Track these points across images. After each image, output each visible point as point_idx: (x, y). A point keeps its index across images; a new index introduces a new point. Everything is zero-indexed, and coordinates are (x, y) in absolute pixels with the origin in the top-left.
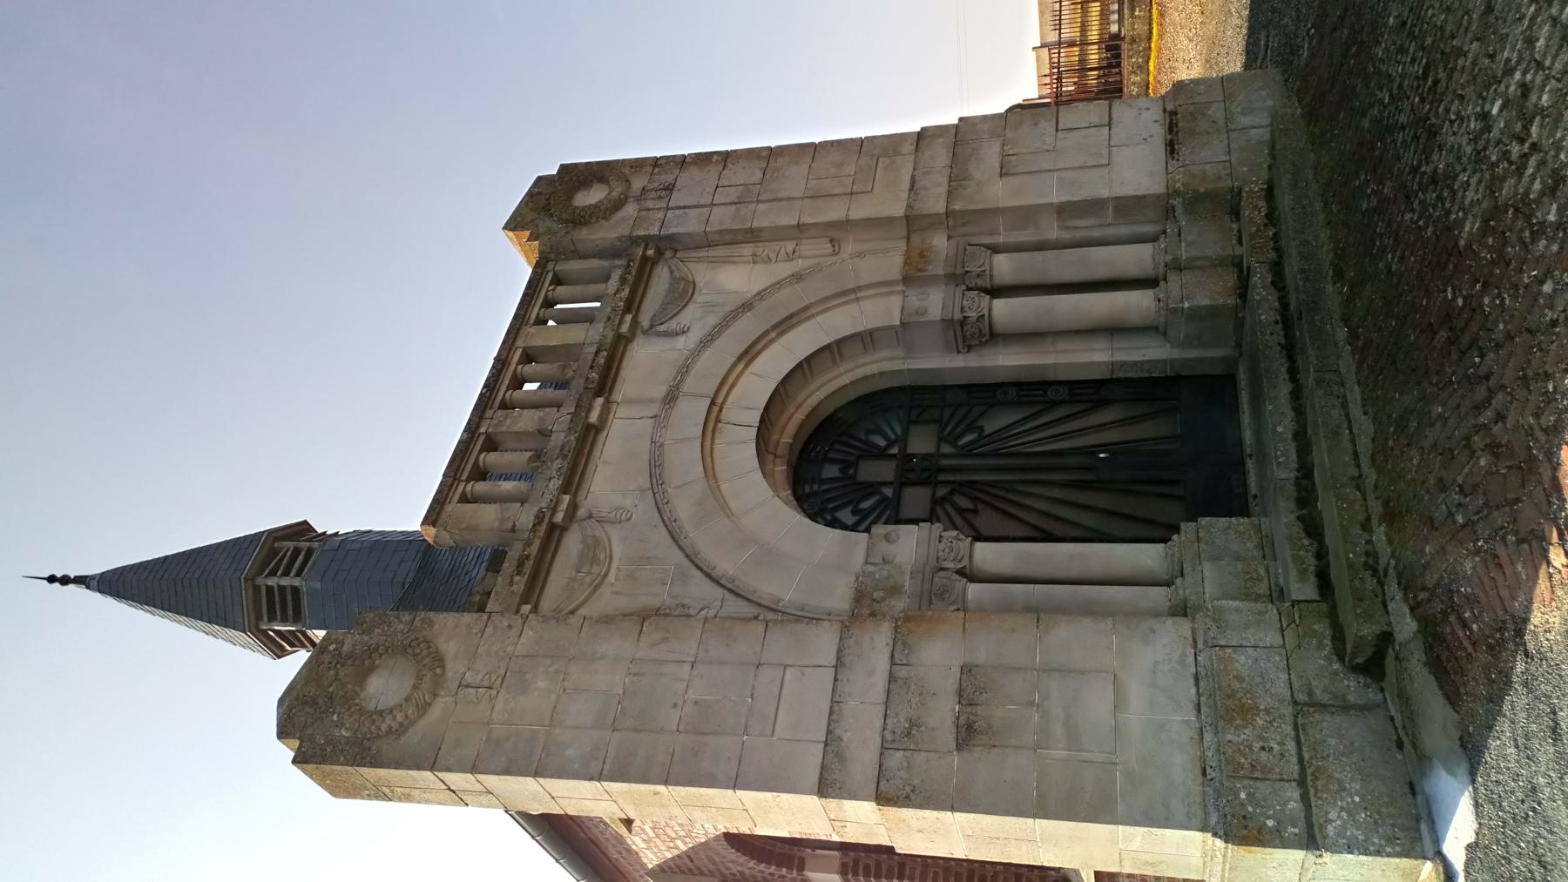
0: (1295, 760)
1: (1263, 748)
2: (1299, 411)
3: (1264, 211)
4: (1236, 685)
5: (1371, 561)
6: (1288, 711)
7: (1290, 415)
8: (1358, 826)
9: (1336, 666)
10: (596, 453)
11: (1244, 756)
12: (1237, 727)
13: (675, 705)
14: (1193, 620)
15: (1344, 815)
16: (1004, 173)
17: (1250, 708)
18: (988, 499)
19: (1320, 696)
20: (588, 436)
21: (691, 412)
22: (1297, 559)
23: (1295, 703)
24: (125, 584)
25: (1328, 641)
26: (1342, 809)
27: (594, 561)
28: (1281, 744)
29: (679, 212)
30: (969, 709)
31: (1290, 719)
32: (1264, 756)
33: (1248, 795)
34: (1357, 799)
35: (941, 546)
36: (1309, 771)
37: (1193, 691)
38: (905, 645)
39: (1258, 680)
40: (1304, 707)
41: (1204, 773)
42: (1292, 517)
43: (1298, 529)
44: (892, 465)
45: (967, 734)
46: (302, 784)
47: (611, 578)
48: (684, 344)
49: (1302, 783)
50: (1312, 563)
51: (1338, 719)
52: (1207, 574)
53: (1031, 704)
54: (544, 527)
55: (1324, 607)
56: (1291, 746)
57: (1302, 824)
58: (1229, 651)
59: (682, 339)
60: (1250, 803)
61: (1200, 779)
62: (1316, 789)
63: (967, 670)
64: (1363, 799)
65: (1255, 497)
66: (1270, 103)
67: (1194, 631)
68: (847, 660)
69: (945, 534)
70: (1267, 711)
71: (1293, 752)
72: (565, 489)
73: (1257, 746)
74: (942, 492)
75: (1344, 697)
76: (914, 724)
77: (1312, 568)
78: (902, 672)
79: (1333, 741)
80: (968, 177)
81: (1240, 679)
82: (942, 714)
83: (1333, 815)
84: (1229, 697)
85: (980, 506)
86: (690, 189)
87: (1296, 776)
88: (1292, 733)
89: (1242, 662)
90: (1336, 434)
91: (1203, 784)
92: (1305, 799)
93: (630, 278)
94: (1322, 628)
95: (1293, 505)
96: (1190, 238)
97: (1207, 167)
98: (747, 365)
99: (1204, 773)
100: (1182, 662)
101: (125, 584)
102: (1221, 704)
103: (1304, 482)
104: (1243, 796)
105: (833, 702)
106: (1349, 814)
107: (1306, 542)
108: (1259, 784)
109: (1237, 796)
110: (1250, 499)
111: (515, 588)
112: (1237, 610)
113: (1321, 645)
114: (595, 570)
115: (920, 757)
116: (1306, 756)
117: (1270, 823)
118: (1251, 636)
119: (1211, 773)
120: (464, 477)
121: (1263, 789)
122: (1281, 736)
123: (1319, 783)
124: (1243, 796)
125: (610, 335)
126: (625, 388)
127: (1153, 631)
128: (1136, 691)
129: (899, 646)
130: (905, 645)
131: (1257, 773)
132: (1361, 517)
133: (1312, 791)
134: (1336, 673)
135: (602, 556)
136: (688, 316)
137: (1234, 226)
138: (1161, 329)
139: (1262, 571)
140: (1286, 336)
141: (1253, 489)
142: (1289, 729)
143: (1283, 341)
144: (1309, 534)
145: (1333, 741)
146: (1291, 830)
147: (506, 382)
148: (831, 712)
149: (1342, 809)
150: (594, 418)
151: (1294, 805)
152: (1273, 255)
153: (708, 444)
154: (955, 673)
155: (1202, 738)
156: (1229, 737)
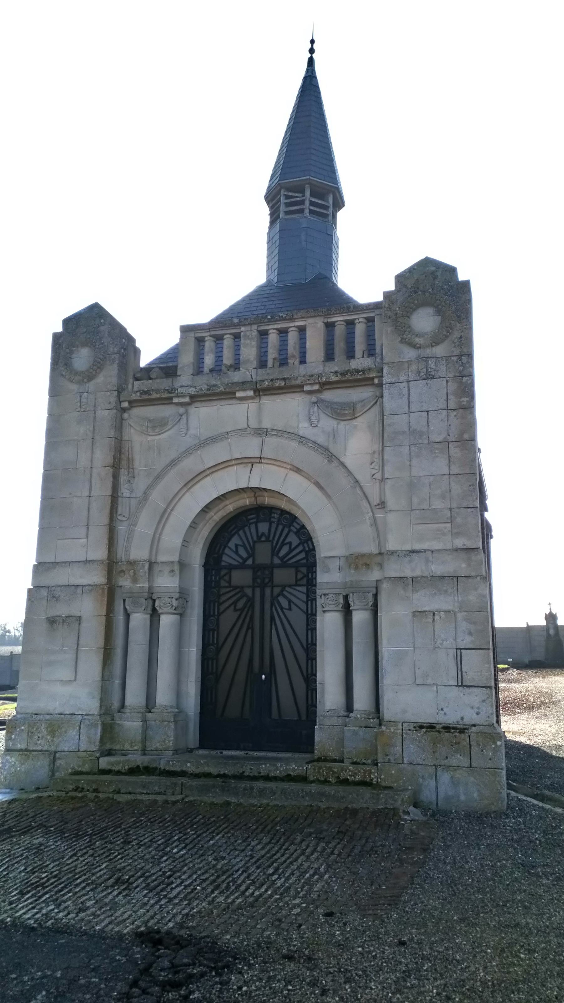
0: (35, 749)
1: (39, 737)
2: (197, 776)
3: (351, 779)
4: (64, 730)
5: (80, 789)
6: (53, 749)
7: (197, 771)
8: (10, 767)
9: (70, 771)
10: (223, 402)
11: (36, 730)
12: (47, 729)
13: (71, 494)
14: (97, 715)
15: (13, 763)
16: (418, 614)
17: (54, 734)
18: (243, 616)
19: (58, 763)
20: (228, 394)
21: (251, 447)
22: (118, 763)
23: (55, 752)
24: (310, 88)
25: (80, 769)
26: (15, 763)
27: (154, 427)
28: (40, 744)
29: (405, 391)
30: (61, 621)
31: (50, 749)
32: (36, 737)
33: (23, 730)
34: (19, 769)
35: (166, 599)
36: (28, 753)
37: (68, 713)
38: (91, 591)
39: (65, 739)
40: (54, 756)
41: (36, 714)
42: (139, 763)
43: (133, 765)
44: (268, 562)
45: (52, 621)
46: (346, 205)
47: (150, 438)
48: (304, 429)
49: (26, 750)
50: (116, 768)
51: (47, 767)
52: (135, 723)
53: (63, 647)
54: (166, 395)
55: (96, 770)
56: (39, 748)
57: (13, 748)
58: (78, 728)
59: (306, 425)
60: (20, 730)
61: (34, 713)
62: (22, 755)
63: (79, 619)
64: (19, 771)
65: (222, 753)
66: (463, 798)
67: (93, 715)
68: (88, 565)
69: (174, 600)
70: (52, 741)
71: (37, 749)
72: (192, 397)
73: (40, 735)
74: (249, 591)
75: (58, 771)
76: (57, 599)
77: (114, 768)
78: (79, 591)
79: (39, 763)
80: (415, 591)
81: (66, 732)
82: (61, 610)
83: (13, 759)
84: (59, 726)
85: (238, 613)
86: (431, 394)
87: (29, 748)
88: (44, 749)
89: (73, 733)
90: (144, 787)
91: (32, 713)
92: (21, 750)
93: (348, 377)
94: (86, 768)
95: (145, 764)
96: (361, 733)
97: (399, 748)
98: (290, 469)
99: (36, 714)
100: (80, 709)
101: (310, 88)
102: (56, 724)
103: (158, 771)
104: (23, 728)
105: (70, 562)
106: (13, 765)
107: (127, 767)
108: (26, 734)
109: (23, 725)
110: (221, 751)
111: (134, 395)
112: (96, 734)
113: (79, 766)
114: (150, 430)
115: (44, 602)
116: (34, 753)
117: (13, 736)
118: (84, 738)
119: (34, 716)
120: (212, 333)
121: (25, 735)
122: (43, 745)
123: (24, 756)
124: (23, 728)
125: (298, 382)
126: (268, 402)
127: (93, 698)
128: (67, 690)
129: (91, 588)
130: (91, 591)
131: (30, 734)
132: (101, 789)
133: (21, 753)
134: (67, 770)
135: (157, 430)
136: (327, 422)
137: (369, 761)
138: (122, 710)
139: (136, 748)
140: (248, 776)
141: (225, 753)
142: (46, 748)
143: (246, 774)
144: (130, 769)
145: (39, 763)
146: (11, 743)
147: (279, 326)
148: (65, 562)
149: (15, 763)
150: (239, 394)
151: (19, 746)
152: (311, 778)
153: (234, 462)
154: (78, 614)
155: (48, 714)
156: (43, 725)
